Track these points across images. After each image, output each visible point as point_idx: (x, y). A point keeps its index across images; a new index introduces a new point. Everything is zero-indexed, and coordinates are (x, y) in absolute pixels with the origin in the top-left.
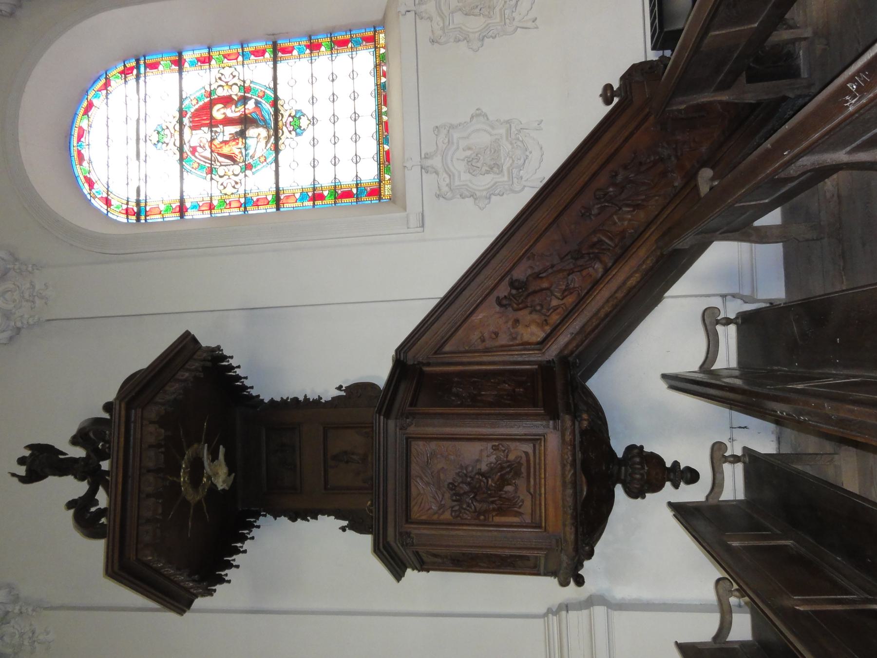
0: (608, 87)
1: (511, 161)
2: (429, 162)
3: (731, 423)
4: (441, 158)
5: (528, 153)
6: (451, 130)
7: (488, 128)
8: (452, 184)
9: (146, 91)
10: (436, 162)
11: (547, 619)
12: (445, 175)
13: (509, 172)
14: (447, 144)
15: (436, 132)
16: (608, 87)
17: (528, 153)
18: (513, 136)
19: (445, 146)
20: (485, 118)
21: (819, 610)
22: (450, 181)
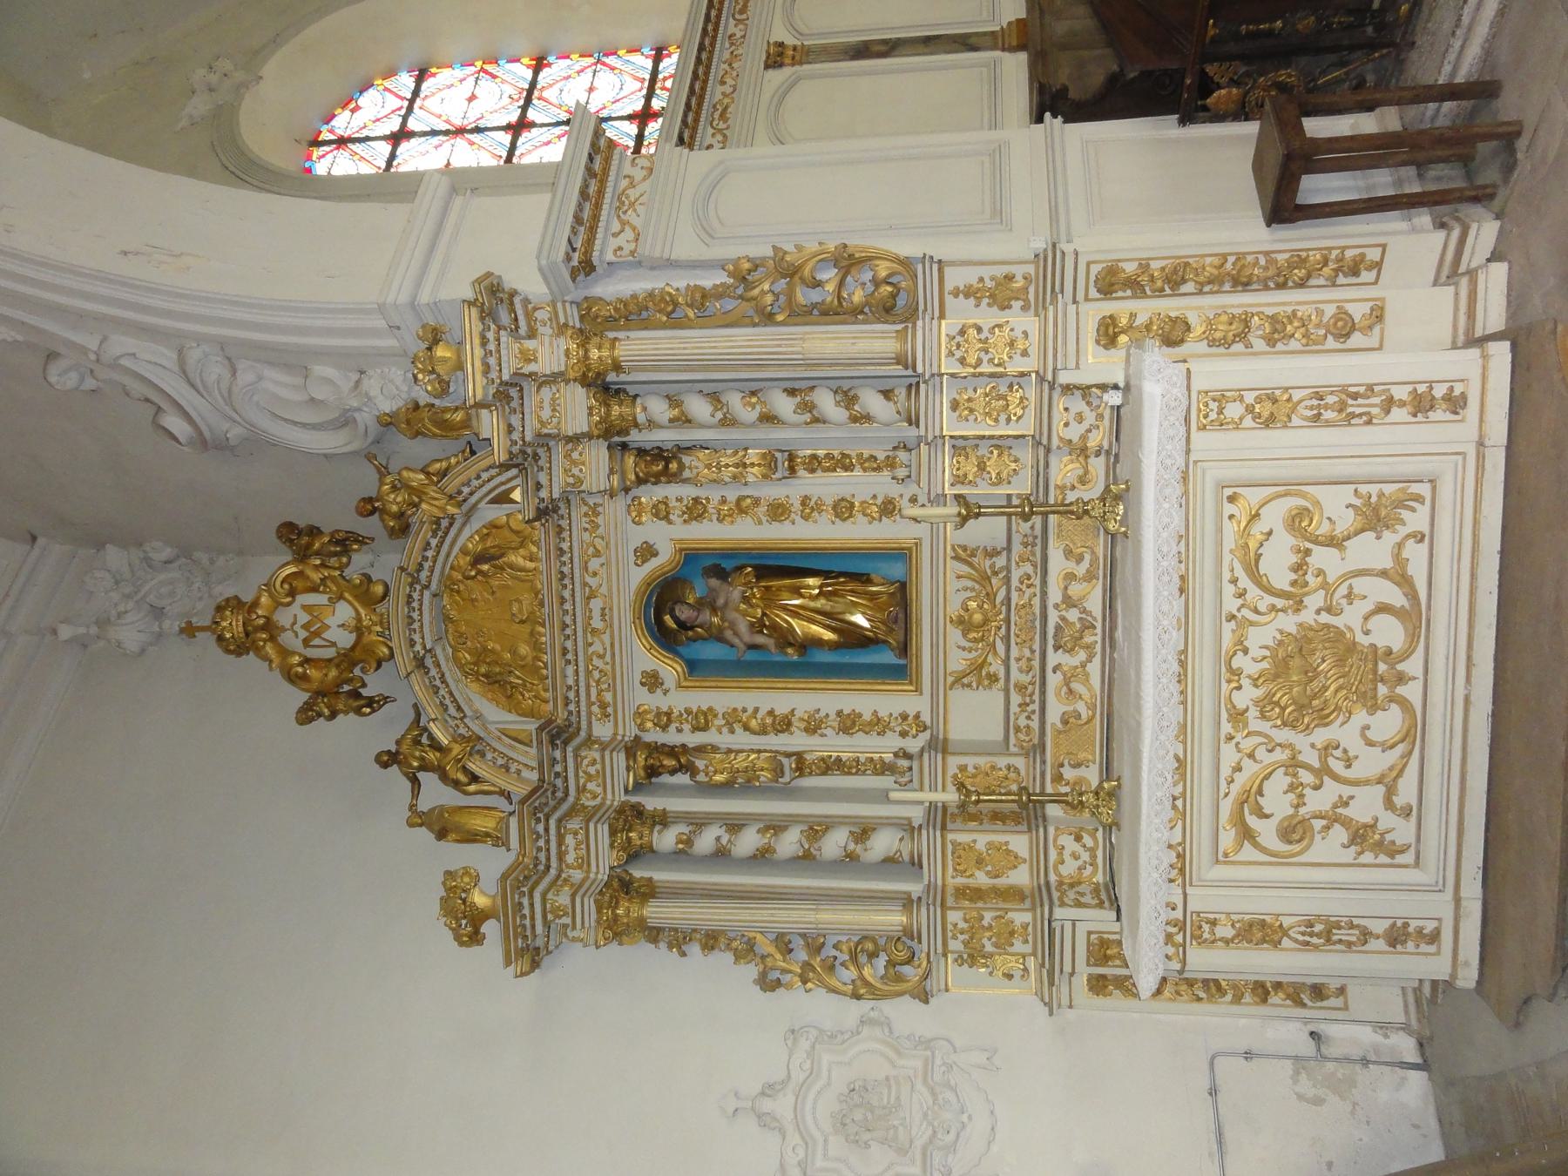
0: (842, 711)
1: (930, 1132)
2: (767, 1105)
3: (952, 264)
4: (794, 1098)
5: (965, 1118)
6: (817, 1046)
7: (891, 1054)
8: (809, 1162)
9: (1268, 1056)
10: (782, 1106)
11: (1478, 230)
12: (797, 1140)
13: (924, 1155)
14: (809, 1072)
15: (790, 1043)
16: (842, 711)
17: (965, 1118)
18: (938, 1077)
19: (802, 1077)
20: (886, 1030)
21: (1411, 1169)
22: (806, 1156)
